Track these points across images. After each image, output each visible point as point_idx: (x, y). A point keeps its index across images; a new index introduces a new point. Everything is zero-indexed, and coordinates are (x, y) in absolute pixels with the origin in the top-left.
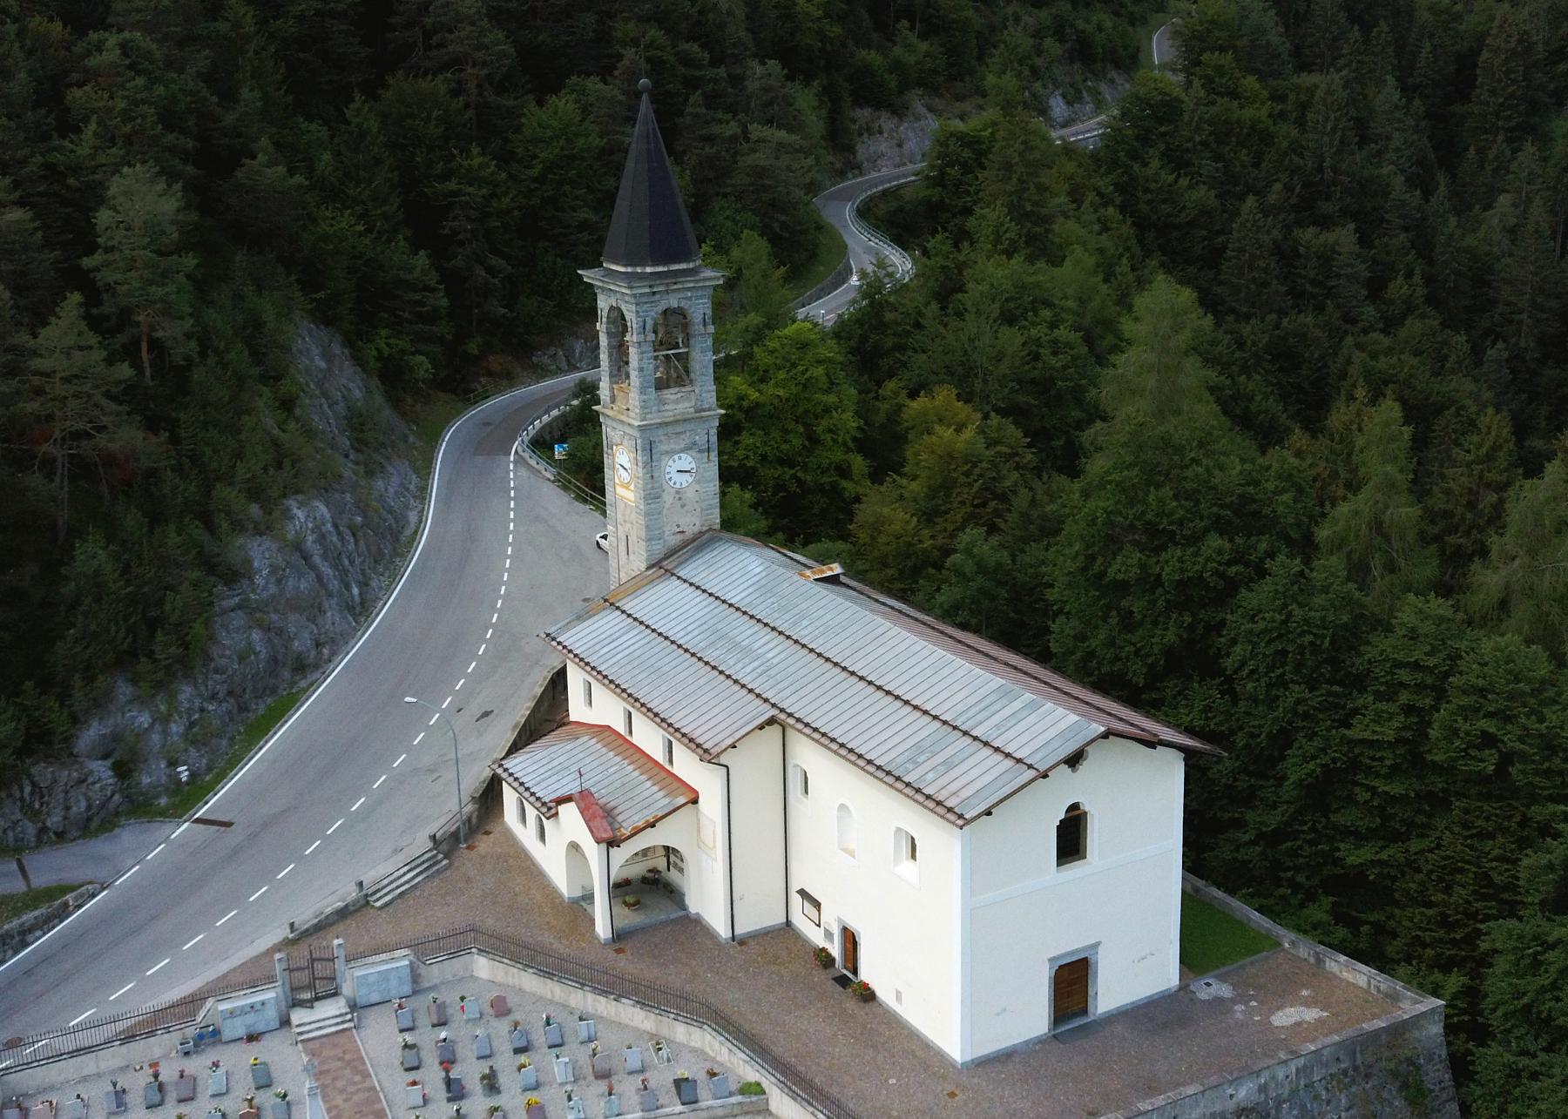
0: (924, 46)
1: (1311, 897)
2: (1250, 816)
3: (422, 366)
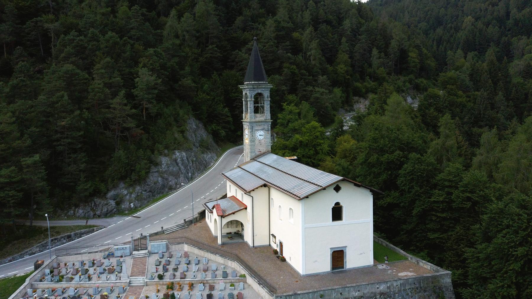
3: (223, 133)
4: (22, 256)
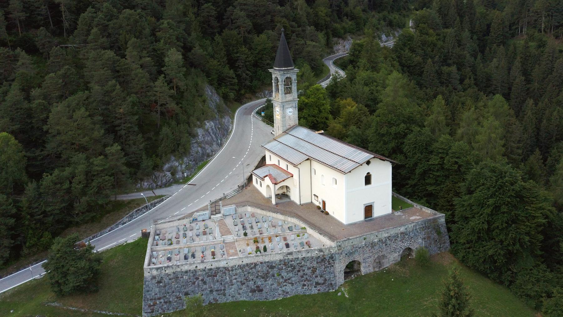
0: (350, 23)
1: (422, 198)
2: (409, 182)
3: (232, 95)
4: (117, 226)
